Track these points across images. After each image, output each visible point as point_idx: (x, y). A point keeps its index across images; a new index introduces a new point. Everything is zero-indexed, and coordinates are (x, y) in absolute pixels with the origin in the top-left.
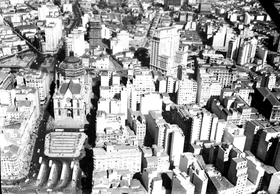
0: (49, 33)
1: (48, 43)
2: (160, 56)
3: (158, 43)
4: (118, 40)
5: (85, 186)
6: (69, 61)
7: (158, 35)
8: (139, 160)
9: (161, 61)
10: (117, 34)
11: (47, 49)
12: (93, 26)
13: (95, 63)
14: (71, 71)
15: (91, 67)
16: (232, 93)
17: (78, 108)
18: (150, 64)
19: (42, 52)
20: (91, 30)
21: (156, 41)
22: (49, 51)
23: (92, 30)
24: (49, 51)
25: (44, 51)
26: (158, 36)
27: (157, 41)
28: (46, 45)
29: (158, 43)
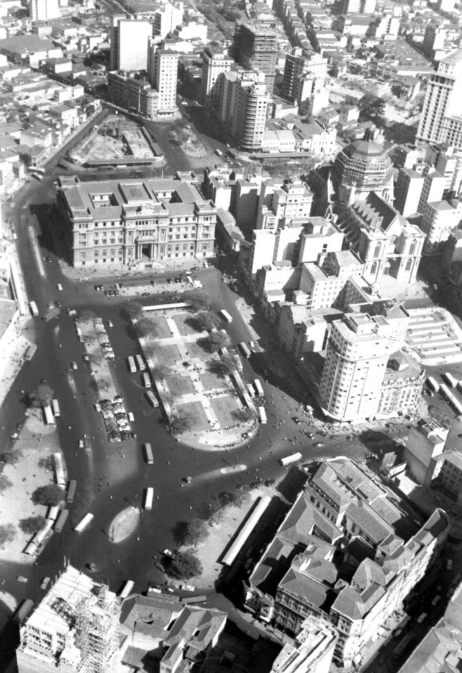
0: (169, 69)
1: (164, 94)
2: (448, 119)
3: (448, 90)
4: (315, 79)
5: (227, 587)
6: (369, 152)
7: (446, 72)
8: (21, 660)
9: (450, 130)
10: (305, 64)
11: (159, 108)
12: (260, 45)
13: (309, 141)
14: (375, 174)
15: (298, 150)
16: (320, 227)
17: (376, 259)
18: (418, 135)
19: (145, 114)
20: (256, 55)
21: (441, 85)
22: (165, 113)
23: (259, 55)
24: (165, 113)
25: (153, 113)
26: (449, 73)
27: (444, 85)
28: (160, 97)
29: (448, 90)
